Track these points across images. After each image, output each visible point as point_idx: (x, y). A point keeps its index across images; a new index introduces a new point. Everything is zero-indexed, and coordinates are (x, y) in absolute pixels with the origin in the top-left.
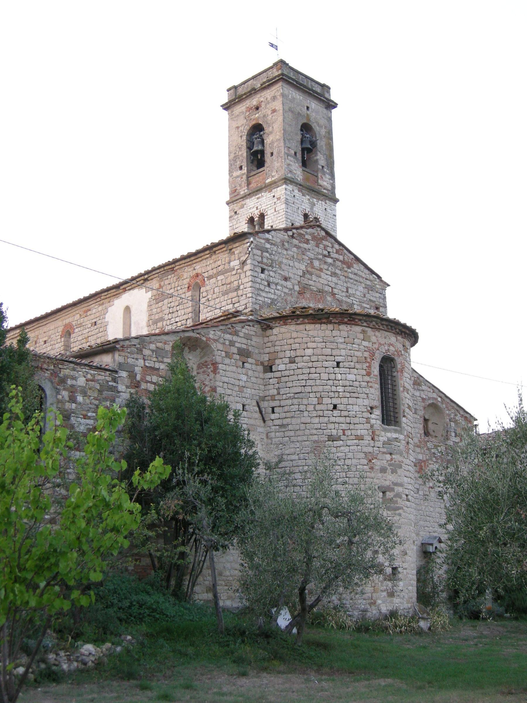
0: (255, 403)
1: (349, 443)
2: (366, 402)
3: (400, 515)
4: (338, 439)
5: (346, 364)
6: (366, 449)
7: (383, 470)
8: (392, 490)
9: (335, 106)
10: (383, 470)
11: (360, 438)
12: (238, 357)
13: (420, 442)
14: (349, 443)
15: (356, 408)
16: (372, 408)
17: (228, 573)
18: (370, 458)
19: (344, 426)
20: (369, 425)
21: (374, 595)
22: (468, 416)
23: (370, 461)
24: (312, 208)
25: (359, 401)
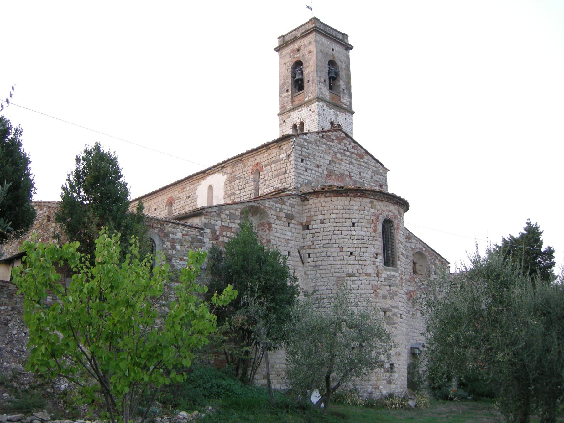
0: (297, 251)
1: (361, 278)
2: (373, 250)
3: (396, 328)
4: (354, 275)
5: (359, 224)
6: (372, 283)
7: (384, 297)
8: (391, 311)
9: (352, 48)
10: (384, 297)
11: (369, 275)
12: (285, 219)
13: (410, 278)
14: (361, 278)
15: (366, 254)
16: (377, 255)
17: (278, 366)
18: (375, 289)
19: (357, 267)
20: (374, 267)
21: (378, 382)
22: (443, 260)
23: (375, 291)
24: (336, 118)
25: (368, 250)
